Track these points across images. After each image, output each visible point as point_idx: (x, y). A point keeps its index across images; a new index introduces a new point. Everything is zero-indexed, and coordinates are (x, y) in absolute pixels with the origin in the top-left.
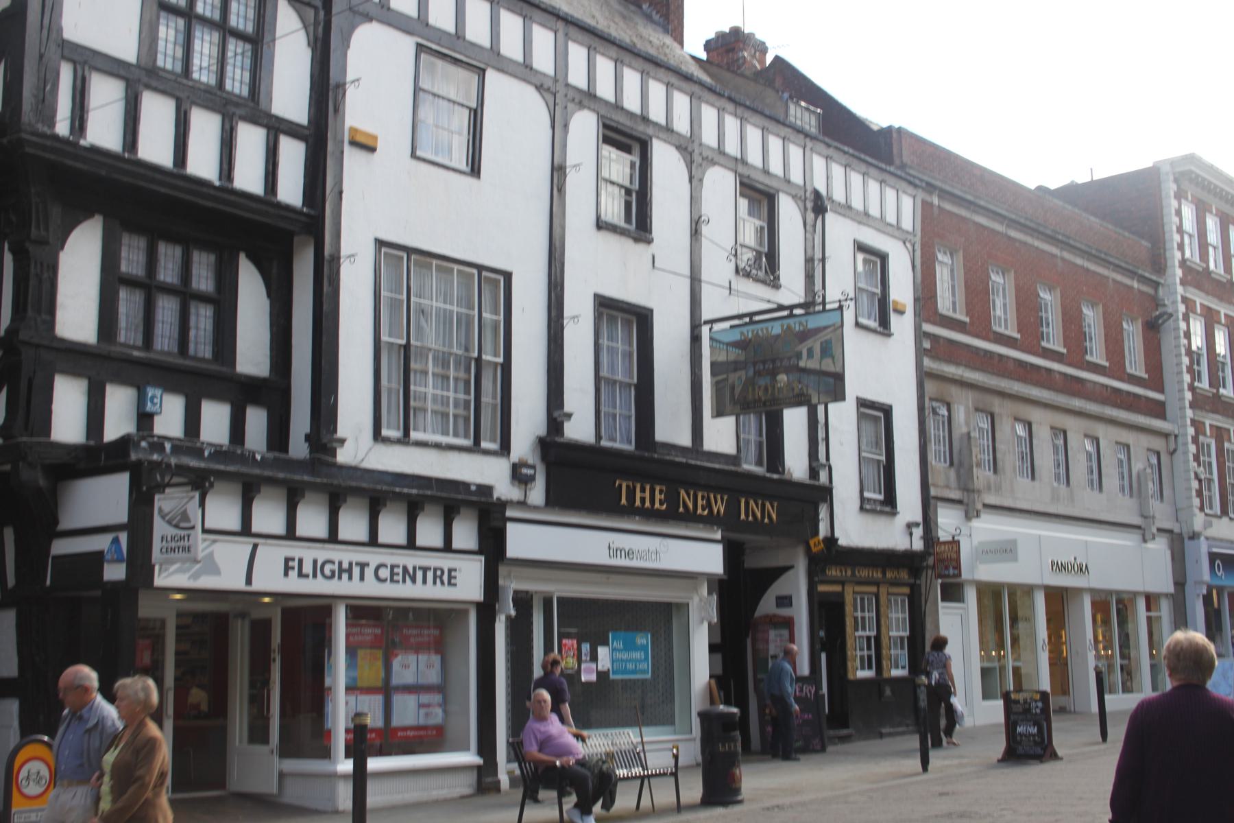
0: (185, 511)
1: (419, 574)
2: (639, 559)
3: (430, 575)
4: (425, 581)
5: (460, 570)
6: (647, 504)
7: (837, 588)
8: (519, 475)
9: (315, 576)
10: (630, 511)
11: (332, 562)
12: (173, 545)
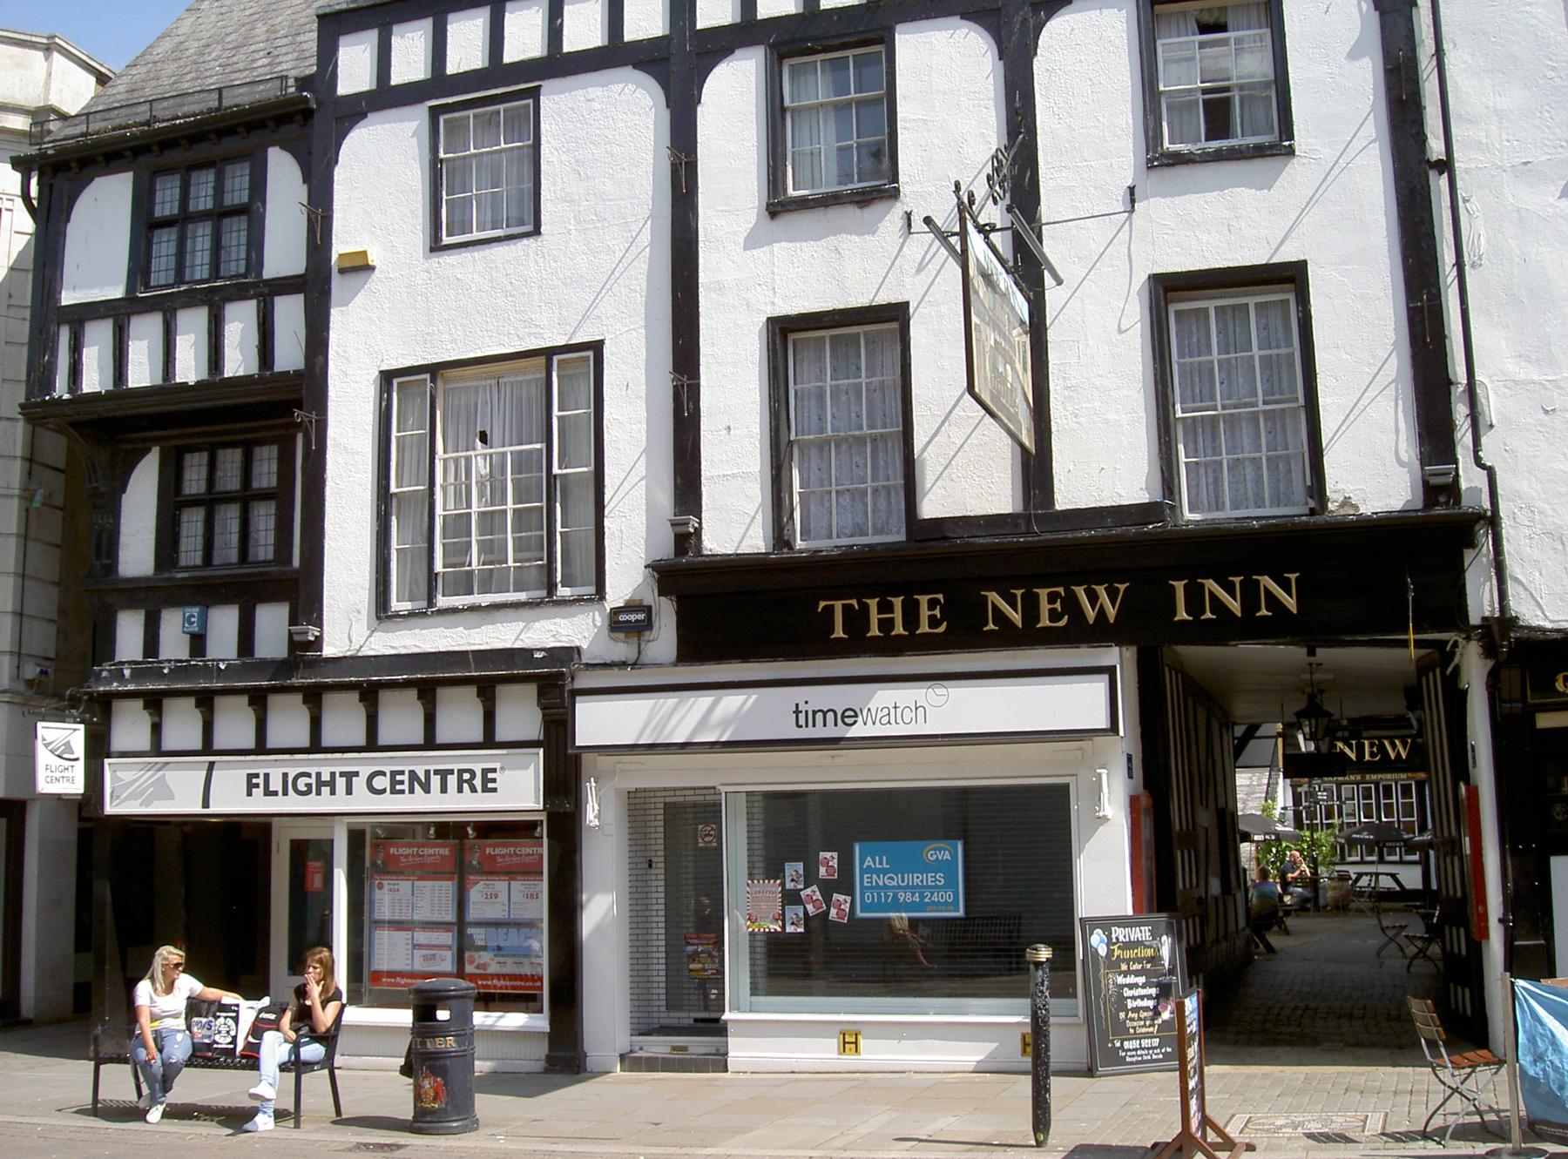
0: (68, 742)
1: (436, 781)
6: (899, 629)
9: (285, 793)
11: (309, 775)
12: (58, 775)
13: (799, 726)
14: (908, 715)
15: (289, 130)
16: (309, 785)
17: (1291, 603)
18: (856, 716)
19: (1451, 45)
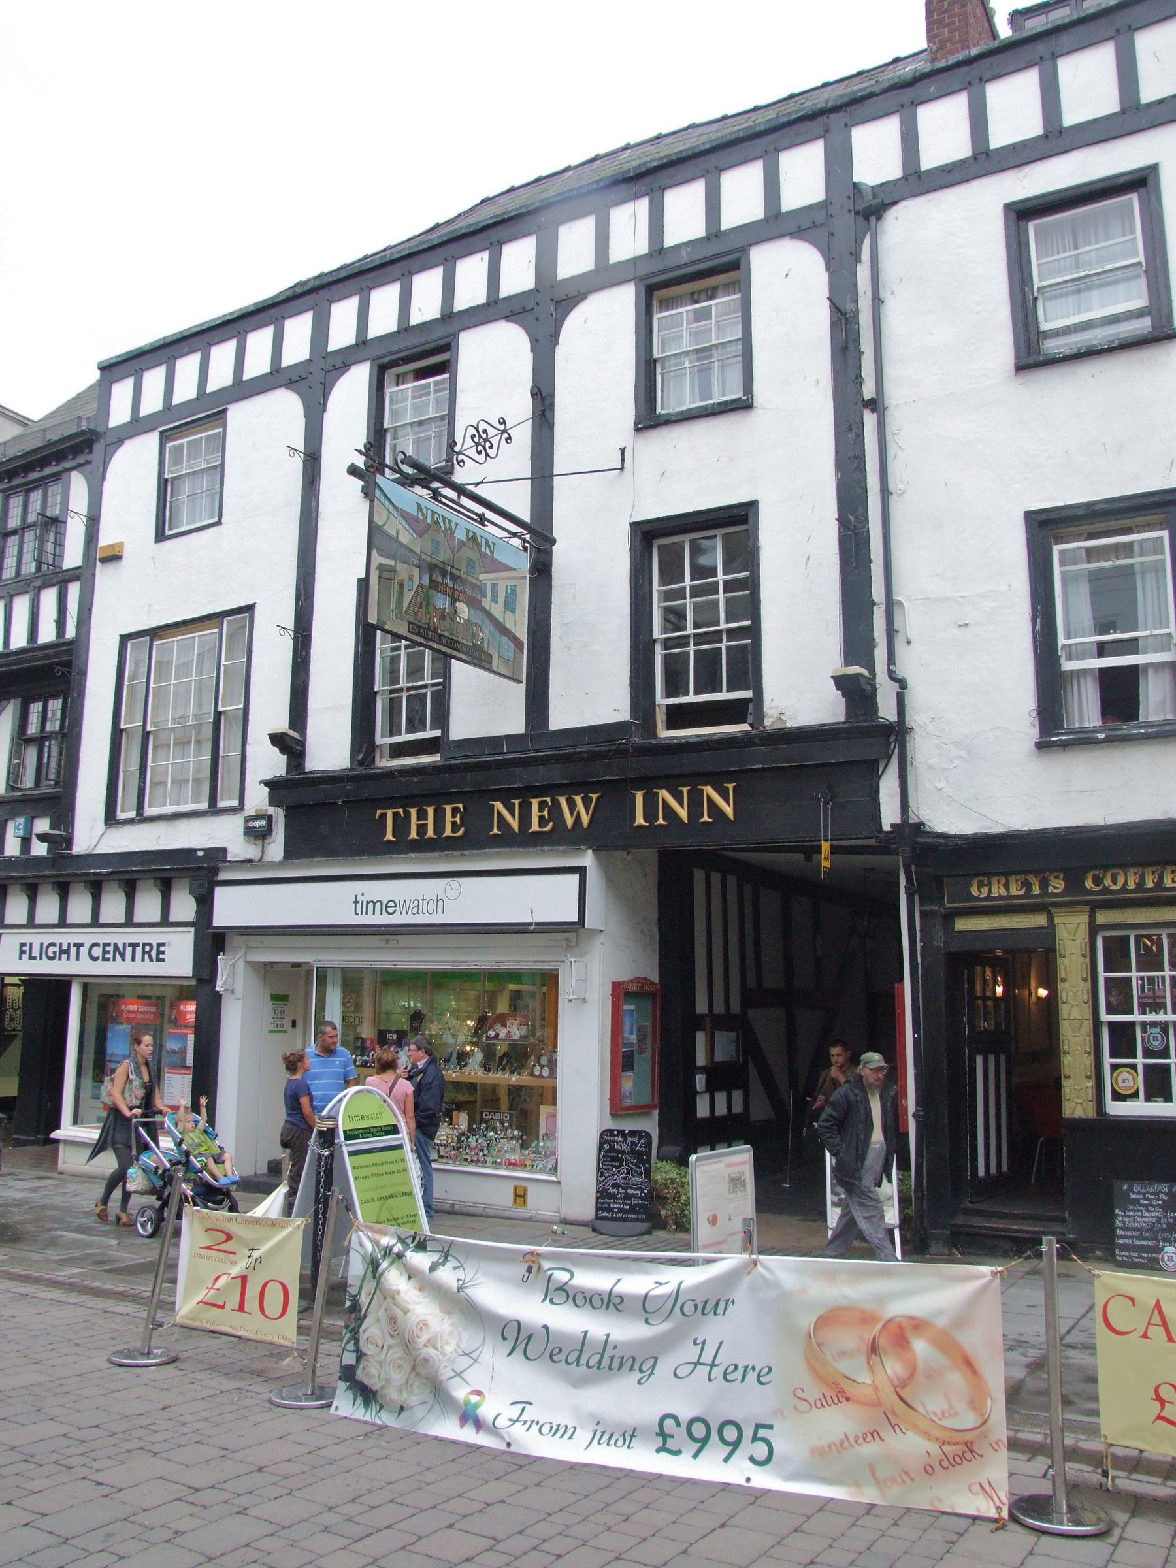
2: (404, 911)
3: (139, 950)
4: (133, 959)
5: (169, 944)
6: (430, 833)
7: (1040, 920)
8: (259, 833)
9: (41, 959)
10: (403, 846)
13: (357, 914)
14: (432, 906)
15: (81, 459)
16: (55, 953)
17: (729, 810)
18: (395, 906)
19: (889, 293)
